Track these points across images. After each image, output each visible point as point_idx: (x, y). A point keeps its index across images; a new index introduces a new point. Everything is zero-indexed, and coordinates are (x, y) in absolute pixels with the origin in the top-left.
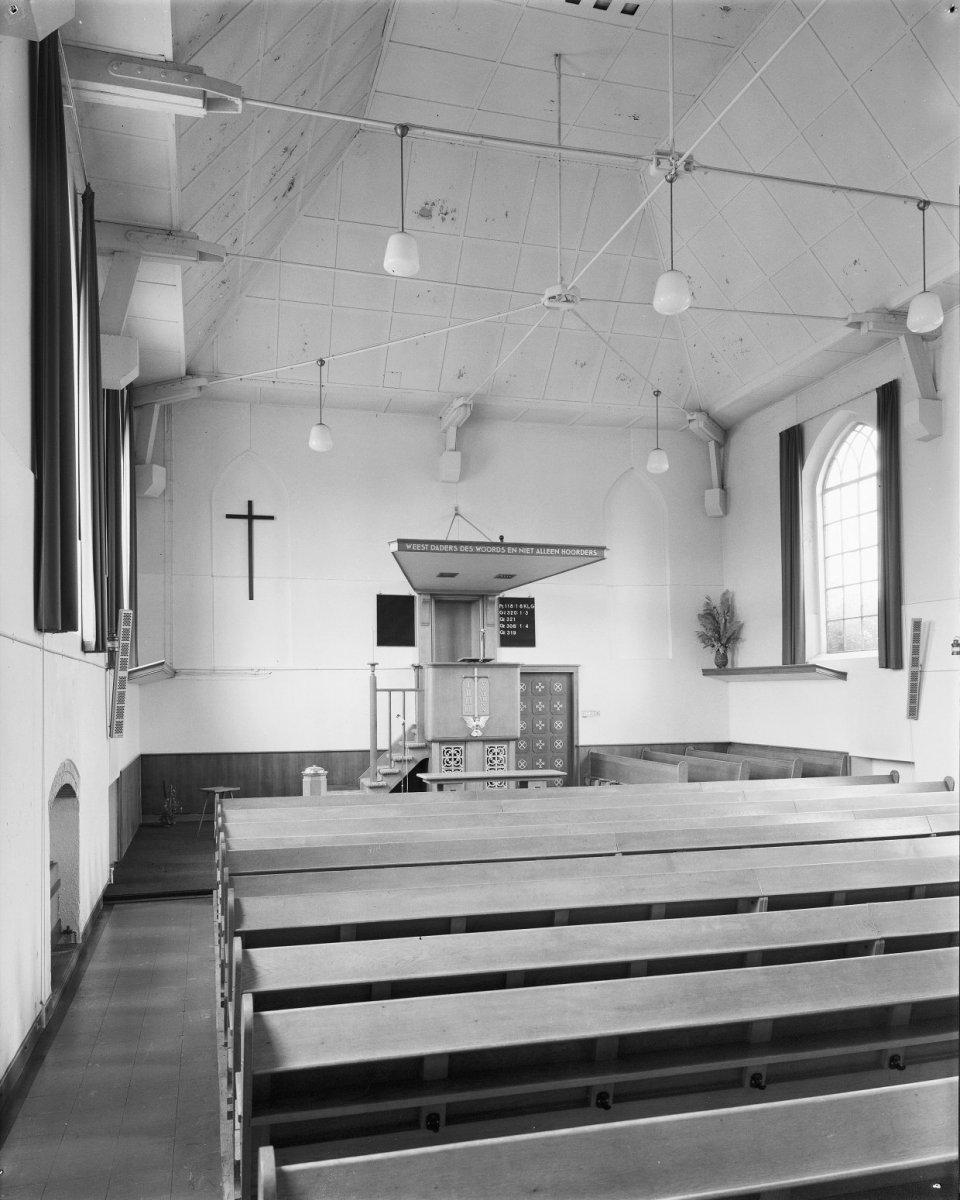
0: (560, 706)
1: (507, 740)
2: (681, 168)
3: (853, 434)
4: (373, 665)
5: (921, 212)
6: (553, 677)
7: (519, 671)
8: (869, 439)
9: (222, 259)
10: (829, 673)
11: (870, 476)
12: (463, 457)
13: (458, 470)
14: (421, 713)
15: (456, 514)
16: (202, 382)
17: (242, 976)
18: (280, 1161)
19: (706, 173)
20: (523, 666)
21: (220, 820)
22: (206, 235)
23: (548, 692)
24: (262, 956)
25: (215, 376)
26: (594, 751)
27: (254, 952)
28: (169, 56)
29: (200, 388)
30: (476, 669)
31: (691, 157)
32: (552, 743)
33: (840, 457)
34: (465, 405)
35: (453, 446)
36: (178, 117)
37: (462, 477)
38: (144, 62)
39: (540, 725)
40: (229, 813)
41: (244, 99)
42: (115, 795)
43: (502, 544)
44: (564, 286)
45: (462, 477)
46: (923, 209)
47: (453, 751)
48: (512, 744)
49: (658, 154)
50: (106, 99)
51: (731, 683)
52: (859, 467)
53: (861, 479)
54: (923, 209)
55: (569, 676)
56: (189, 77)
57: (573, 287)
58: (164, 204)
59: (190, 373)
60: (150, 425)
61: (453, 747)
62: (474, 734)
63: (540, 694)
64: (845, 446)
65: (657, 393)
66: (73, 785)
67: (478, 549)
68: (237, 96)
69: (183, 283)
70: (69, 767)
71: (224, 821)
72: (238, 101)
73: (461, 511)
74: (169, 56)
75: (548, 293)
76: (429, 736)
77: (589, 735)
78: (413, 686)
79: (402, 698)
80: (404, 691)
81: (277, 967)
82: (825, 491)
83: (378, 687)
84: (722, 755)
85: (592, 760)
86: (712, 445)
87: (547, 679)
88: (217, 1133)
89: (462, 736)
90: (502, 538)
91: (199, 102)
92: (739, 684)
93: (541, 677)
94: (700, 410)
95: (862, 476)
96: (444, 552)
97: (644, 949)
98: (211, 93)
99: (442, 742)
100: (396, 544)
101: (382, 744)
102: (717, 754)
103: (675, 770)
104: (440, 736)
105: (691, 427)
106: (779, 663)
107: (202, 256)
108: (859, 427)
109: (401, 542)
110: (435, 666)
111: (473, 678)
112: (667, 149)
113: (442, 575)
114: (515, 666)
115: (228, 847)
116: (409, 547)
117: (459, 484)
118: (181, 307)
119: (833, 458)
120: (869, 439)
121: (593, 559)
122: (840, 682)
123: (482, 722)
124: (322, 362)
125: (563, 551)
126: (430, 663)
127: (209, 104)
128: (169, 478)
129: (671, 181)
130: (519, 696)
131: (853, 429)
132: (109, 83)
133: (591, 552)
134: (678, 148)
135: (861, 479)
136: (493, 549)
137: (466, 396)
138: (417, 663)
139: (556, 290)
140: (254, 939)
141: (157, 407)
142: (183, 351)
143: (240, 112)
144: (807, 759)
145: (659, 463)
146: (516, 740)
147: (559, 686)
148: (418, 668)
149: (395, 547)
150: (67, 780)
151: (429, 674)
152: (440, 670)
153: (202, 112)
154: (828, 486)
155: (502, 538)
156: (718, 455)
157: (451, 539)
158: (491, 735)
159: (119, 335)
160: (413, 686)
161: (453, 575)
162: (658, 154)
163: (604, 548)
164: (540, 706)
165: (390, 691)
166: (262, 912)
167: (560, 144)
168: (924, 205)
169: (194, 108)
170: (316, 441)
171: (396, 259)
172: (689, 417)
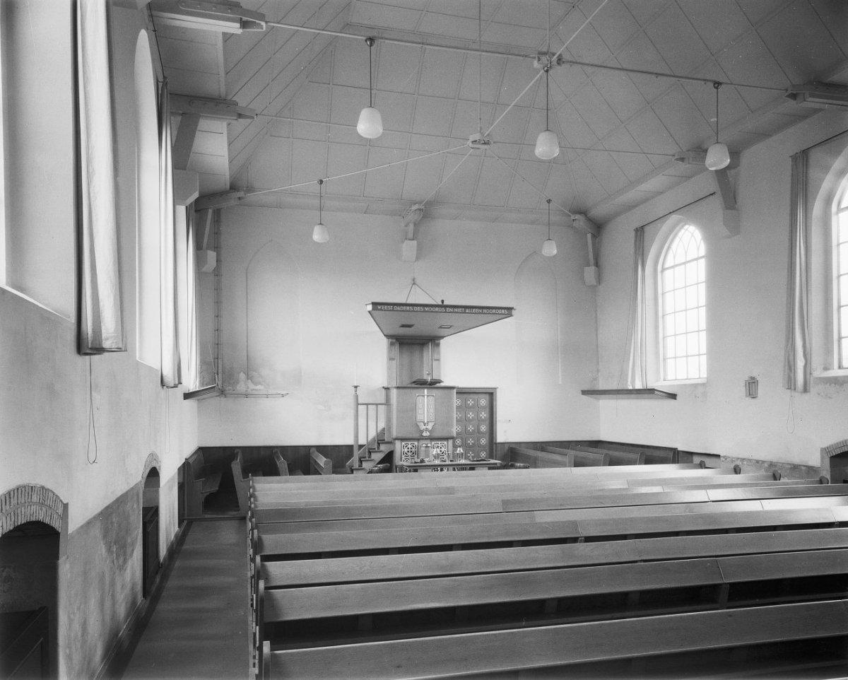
0: (484, 415)
1: (447, 439)
2: (555, 63)
4: (356, 387)
5: (716, 90)
6: (481, 396)
7: (455, 391)
8: (692, 235)
9: (253, 118)
10: (664, 394)
12: (419, 245)
13: (415, 252)
14: (389, 420)
15: (414, 284)
16: (241, 194)
17: (261, 574)
18: (272, 649)
19: (571, 65)
20: (458, 388)
21: (251, 490)
22: (242, 100)
23: (476, 407)
24: (272, 566)
25: (250, 189)
26: (514, 446)
27: (268, 564)
29: (239, 198)
30: (426, 390)
31: (560, 55)
32: (478, 440)
33: (674, 246)
34: (420, 210)
35: (411, 236)
36: (224, 34)
37: (418, 258)
39: (471, 428)
40: (258, 486)
41: (266, 22)
42: (494, 433)
43: (443, 306)
44: (482, 134)
45: (418, 258)
46: (717, 88)
47: (410, 446)
48: (451, 442)
49: (539, 53)
50: (177, 23)
51: (601, 401)
53: (684, 263)
54: (717, 88)
55: (491, 394)
56: (230, 9)
57: (488, 135)
58: (215, 84)
59: (234, 187)
60: (206, 220)
61: (410, 443)
62: (424, 434)
63: (471, 407)
64: (677, 240)
65: (549, 201)
66: (157, 468)
67: (426, 309)
68: (263, 21)
69: (228, 133)
70: (153, 456)
71: (254, 490)
72: (263, 24)
73: (418, 281)
75: (472, 138)
76: (395, 434)
77: (504, 435)
78: (384, 402)
79: (376, 409)
80: (377, 405)
81: (278, 570)
82: (663, 270)
83: (360, 402)
84: (595, 450)
85: (511, 452)
86: (589, 236)
87: (476, 396)
89: (417, 436)
90: (443, 301)
91: (238, 25)
93: (471, 396)
94: (580, 213)
95: (676, 263)
96: (403, 311)
98: (245, 19)
99: (402, 439)
100: (371, 306)
101: (362, 441)
102: (591, 449)
103: (566, 459)
104: (400, 436)
105: (574, 225)
107: (240, 116)
109: (375, 304)
110: (398, 388)
111: (424, 396)
112: (545, 50)
113: (403, 326)
114: (452, 388)
115: (256, 506)
116: (379, 307)
117: (416, 263)
118: (226, 145)
119: (669, 248)
120: (692, 235)
122: (672, 401)
123: (430, 427)
124: (321, 182)
125: (485, 311)
126: (395, 385)
127: (244, 25)
128: (218, 261)
129: (547, 71)
130: (455, 409)
132: (178, 13)
133: (503, 311)
134: (553, 50)
136: (437, 309)
137: (420, 203)
138: (386, 385)
139: (477, 137)
140: (267, 558)
141: (210, 211)
142: (228, 174)
143: (264, 29)
144: (649, 452)
145: (551, 249)
146: (452, 438)
147: (484, 401)
148: (387, 389)
149: (370, 308)
150: (154, 464)
151: (394, 392)
152: (402, 390)
153: (240, 31)
154: (666, 266)
155: (443, 301)
156: (594, 244)
157: (410, 301)
158: (436, 435)
159: (185, 170)
160: (384, 402)
161: (410, 326)
162: (539, 53)
163: (512, 309)
164: (471, 415)
165: (367, 404)
166: (272, 542)
168: (717, 84)
169: (234, 28)
170: (318, 235)
171: (318, 235)
172: (573, 218)
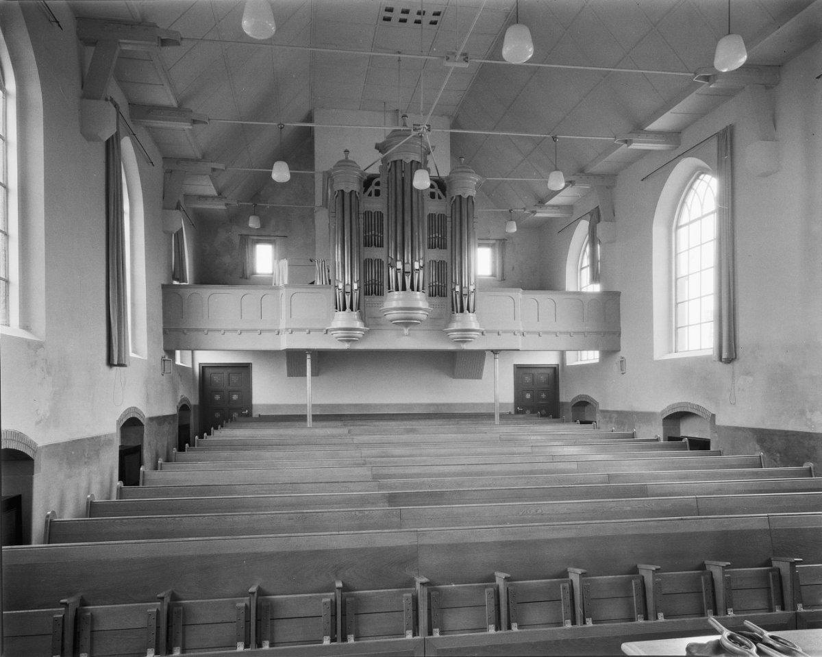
3: (698, 181)
8: (708, 186)
11: (712, 213)
28: (175, 105)
33: (689, 200)
38: (167, 108)
52: (702, 205)
53: (703, 217)
64: (692, 192)
74: (175, 105)
82: (678, 227)
88: (578, 567)
92: (713, 331)
97: (732, 475)
106: (567, 352)
108: (702, 176)
120: (708, 186)
121: (702, 200)
131: (697, 178)
135: (703, 217)
167: (347, 158)
